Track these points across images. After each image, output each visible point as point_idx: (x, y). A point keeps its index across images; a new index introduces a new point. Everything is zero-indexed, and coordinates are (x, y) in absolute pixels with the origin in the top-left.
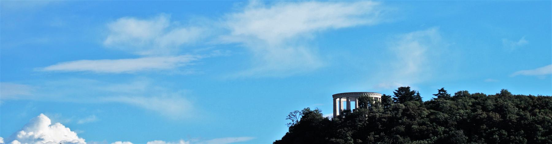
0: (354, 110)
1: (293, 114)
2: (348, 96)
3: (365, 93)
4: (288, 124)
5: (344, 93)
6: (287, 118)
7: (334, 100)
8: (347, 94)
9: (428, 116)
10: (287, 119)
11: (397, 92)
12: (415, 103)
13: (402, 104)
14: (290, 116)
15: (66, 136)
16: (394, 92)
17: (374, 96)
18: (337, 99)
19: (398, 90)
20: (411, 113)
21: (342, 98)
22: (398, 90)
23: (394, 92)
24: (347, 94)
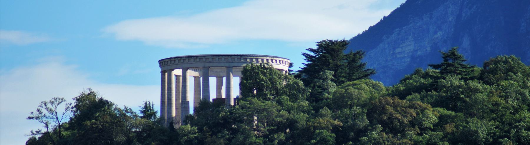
0: (213, 100)
1: (49, 106)
2: (207, 65)
3: (251, 57)
4: (34, 132)
5: (197, 57)
6: (31, 116)
7: (163, 73)
8: (204, 59)
9: (438, 126)
10: (29, 118)
11: (312, 54)
12: (374, 86)
13: (333, 92)
14: (41, 113)
15: (27, 136)
16: (304, 54)
17: (276, 66)
18: (173, 70)
19: (315, 47)
20: (391, 118)
21: (188, 68)
22: (315, 47)
23: (304, 54)
24: (204, 59)
